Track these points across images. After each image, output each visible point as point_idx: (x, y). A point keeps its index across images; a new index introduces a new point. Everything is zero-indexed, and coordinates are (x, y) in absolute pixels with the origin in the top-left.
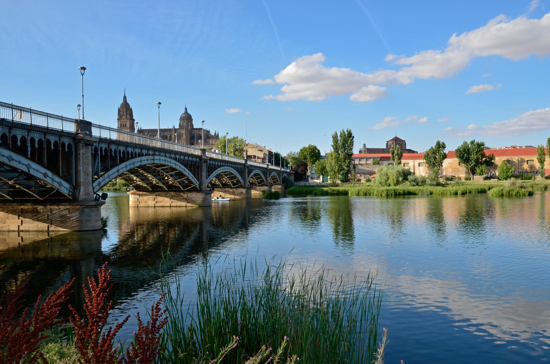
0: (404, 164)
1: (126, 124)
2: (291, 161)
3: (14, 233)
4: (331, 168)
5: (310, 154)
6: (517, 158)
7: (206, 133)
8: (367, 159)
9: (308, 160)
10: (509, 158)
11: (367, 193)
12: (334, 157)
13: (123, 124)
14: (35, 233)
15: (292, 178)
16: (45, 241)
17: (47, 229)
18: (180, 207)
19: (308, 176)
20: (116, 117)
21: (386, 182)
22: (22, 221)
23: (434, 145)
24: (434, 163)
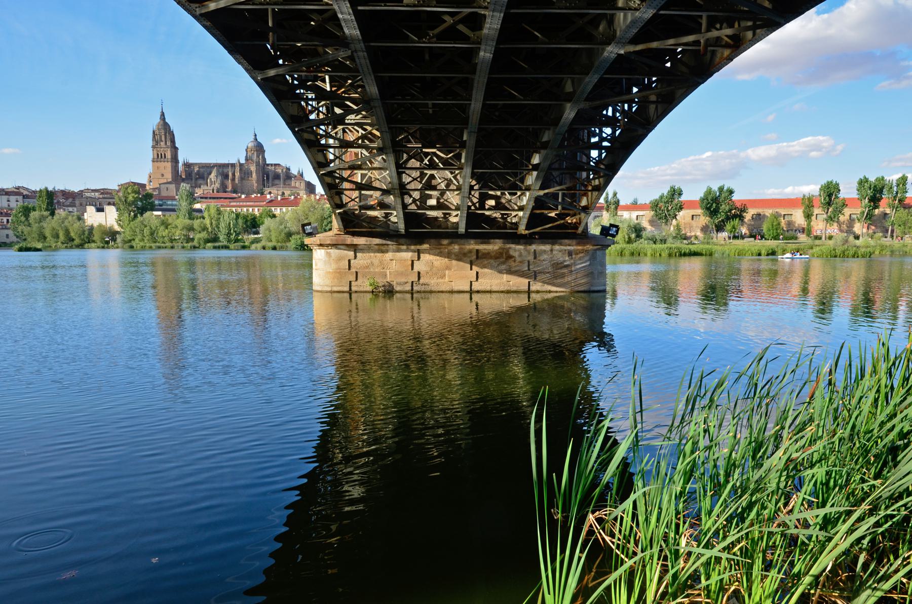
3: (461, 295)
6: (770, 211)
7: (286, 171)
10: (760, 211)
13: (161, 154)
16: (520, 309)
20: (150, 143)
22: (477, 273)
23: (665, 191)
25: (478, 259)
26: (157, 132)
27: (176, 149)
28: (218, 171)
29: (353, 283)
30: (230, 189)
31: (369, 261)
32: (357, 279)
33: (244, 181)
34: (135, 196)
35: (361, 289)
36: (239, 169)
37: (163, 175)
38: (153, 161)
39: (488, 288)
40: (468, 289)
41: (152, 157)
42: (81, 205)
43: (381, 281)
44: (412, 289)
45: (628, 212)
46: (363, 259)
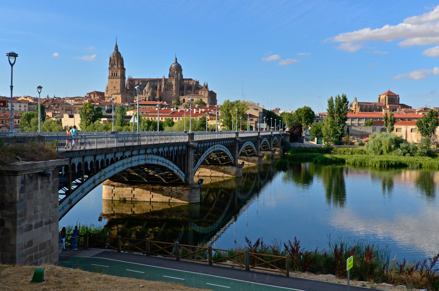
0: (397, 129)
1: (117, 73)
2: (287, 123)
3: (147, 203)
4: (326, 133)
5: (304, 116)
7: (196, 84)
8: (360, 119)
9: (303, 121)
11: (363, 163)
12: (329, 122)
13: (114, 73)
14: (160, 203)
15: (288, 139)
17: (168, 201)
18: (218, 177)
19: (303, 137)
20: (108, 66)
21: (379, 148)
22: (152, 195)
24: (426, 131)
25: (153, 190)
26: (112, 59)
27: (124, 69)
28: (150, 84)
29: (113, 197)
30: (158, 97)
31: (118, 190)
32: (114, 196)
33: (167, 91)
34: (91, 110)
35: (116, 199)
36: (164, 83)
37: (115, 87)
38: (109, 78)
39: (156, 201)
40: (149, 200)
41: (108, 75)
42: (62, 109)
43: (122, 197)
44: (132, 200)
45: (405, 126)
46: (116, 189)
